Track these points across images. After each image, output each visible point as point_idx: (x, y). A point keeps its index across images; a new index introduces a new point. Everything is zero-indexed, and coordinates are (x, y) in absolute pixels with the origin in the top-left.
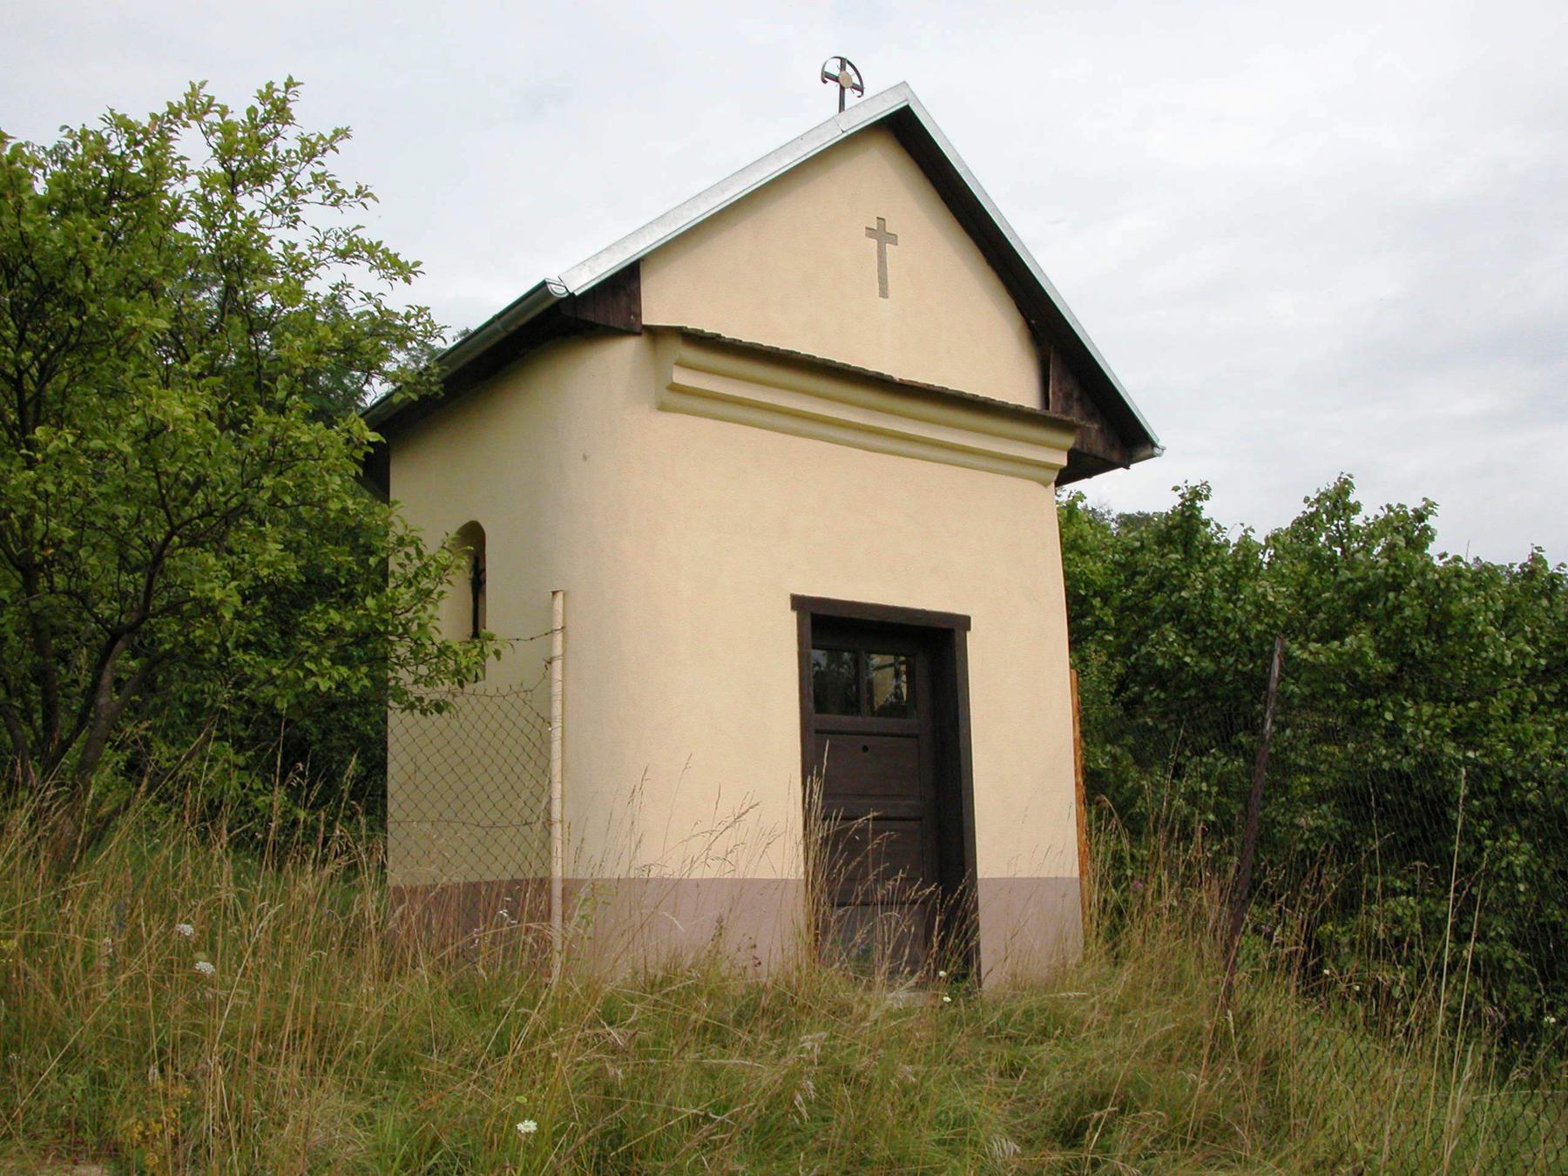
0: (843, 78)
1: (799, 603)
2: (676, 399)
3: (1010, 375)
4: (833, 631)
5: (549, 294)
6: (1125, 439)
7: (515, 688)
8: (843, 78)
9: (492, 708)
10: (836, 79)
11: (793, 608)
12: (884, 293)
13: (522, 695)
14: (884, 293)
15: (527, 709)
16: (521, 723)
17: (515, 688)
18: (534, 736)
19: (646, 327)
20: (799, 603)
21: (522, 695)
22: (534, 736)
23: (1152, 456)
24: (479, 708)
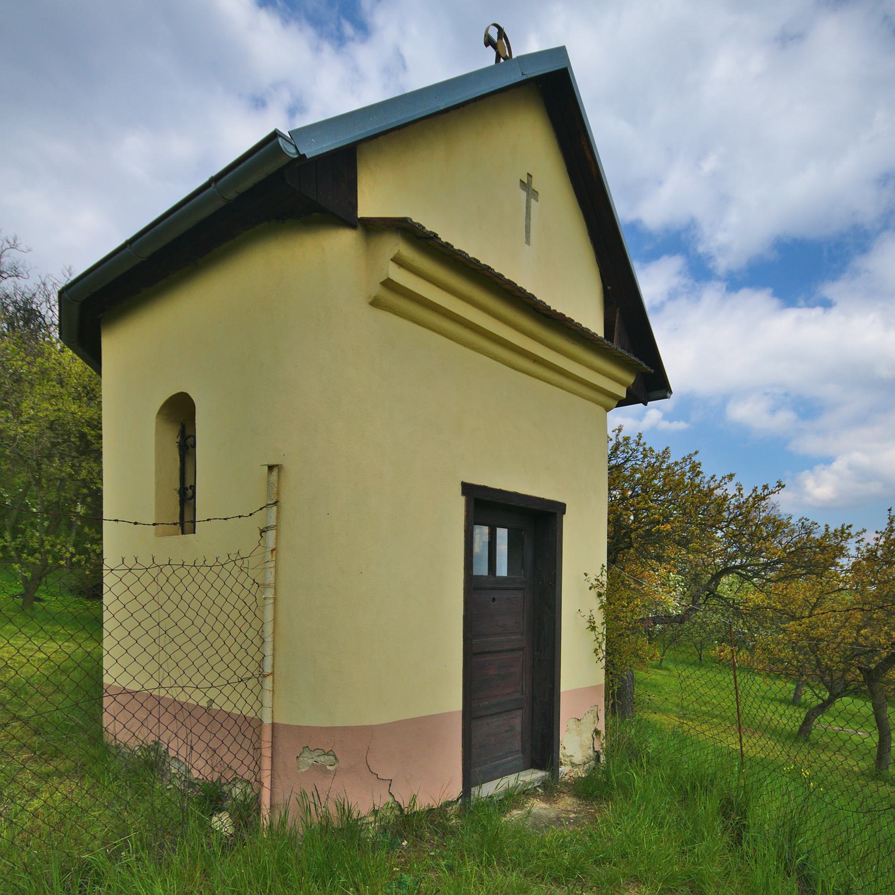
0: (497, 41)
1: (468, 489)
2: (390, 297)
3: (591, 316)
4: (485, 505)
5: (279, 150)
6: (650, 383)
7: (233, 557)
8: (497, 41)
9: (212, 577)
10: (495, 46)
11: (463, 493)
12: (528, 242)
13: (239, 563)
14: (528, 242)
15: (243, 575)
16: (238, 589)
17: (233, 557)
18: (250, 600)
19: (362, 219)
20: (468, 489)
21: (239, 563)
22: (250, 600)
23: (666, 397)
24: (199, 579)
